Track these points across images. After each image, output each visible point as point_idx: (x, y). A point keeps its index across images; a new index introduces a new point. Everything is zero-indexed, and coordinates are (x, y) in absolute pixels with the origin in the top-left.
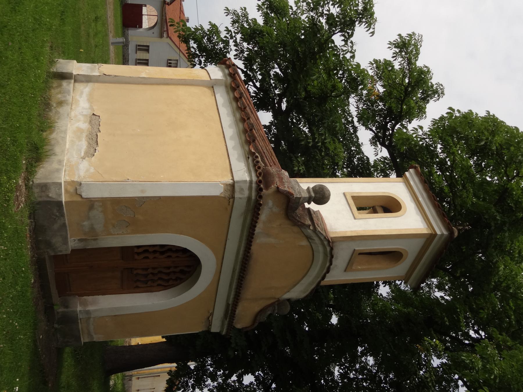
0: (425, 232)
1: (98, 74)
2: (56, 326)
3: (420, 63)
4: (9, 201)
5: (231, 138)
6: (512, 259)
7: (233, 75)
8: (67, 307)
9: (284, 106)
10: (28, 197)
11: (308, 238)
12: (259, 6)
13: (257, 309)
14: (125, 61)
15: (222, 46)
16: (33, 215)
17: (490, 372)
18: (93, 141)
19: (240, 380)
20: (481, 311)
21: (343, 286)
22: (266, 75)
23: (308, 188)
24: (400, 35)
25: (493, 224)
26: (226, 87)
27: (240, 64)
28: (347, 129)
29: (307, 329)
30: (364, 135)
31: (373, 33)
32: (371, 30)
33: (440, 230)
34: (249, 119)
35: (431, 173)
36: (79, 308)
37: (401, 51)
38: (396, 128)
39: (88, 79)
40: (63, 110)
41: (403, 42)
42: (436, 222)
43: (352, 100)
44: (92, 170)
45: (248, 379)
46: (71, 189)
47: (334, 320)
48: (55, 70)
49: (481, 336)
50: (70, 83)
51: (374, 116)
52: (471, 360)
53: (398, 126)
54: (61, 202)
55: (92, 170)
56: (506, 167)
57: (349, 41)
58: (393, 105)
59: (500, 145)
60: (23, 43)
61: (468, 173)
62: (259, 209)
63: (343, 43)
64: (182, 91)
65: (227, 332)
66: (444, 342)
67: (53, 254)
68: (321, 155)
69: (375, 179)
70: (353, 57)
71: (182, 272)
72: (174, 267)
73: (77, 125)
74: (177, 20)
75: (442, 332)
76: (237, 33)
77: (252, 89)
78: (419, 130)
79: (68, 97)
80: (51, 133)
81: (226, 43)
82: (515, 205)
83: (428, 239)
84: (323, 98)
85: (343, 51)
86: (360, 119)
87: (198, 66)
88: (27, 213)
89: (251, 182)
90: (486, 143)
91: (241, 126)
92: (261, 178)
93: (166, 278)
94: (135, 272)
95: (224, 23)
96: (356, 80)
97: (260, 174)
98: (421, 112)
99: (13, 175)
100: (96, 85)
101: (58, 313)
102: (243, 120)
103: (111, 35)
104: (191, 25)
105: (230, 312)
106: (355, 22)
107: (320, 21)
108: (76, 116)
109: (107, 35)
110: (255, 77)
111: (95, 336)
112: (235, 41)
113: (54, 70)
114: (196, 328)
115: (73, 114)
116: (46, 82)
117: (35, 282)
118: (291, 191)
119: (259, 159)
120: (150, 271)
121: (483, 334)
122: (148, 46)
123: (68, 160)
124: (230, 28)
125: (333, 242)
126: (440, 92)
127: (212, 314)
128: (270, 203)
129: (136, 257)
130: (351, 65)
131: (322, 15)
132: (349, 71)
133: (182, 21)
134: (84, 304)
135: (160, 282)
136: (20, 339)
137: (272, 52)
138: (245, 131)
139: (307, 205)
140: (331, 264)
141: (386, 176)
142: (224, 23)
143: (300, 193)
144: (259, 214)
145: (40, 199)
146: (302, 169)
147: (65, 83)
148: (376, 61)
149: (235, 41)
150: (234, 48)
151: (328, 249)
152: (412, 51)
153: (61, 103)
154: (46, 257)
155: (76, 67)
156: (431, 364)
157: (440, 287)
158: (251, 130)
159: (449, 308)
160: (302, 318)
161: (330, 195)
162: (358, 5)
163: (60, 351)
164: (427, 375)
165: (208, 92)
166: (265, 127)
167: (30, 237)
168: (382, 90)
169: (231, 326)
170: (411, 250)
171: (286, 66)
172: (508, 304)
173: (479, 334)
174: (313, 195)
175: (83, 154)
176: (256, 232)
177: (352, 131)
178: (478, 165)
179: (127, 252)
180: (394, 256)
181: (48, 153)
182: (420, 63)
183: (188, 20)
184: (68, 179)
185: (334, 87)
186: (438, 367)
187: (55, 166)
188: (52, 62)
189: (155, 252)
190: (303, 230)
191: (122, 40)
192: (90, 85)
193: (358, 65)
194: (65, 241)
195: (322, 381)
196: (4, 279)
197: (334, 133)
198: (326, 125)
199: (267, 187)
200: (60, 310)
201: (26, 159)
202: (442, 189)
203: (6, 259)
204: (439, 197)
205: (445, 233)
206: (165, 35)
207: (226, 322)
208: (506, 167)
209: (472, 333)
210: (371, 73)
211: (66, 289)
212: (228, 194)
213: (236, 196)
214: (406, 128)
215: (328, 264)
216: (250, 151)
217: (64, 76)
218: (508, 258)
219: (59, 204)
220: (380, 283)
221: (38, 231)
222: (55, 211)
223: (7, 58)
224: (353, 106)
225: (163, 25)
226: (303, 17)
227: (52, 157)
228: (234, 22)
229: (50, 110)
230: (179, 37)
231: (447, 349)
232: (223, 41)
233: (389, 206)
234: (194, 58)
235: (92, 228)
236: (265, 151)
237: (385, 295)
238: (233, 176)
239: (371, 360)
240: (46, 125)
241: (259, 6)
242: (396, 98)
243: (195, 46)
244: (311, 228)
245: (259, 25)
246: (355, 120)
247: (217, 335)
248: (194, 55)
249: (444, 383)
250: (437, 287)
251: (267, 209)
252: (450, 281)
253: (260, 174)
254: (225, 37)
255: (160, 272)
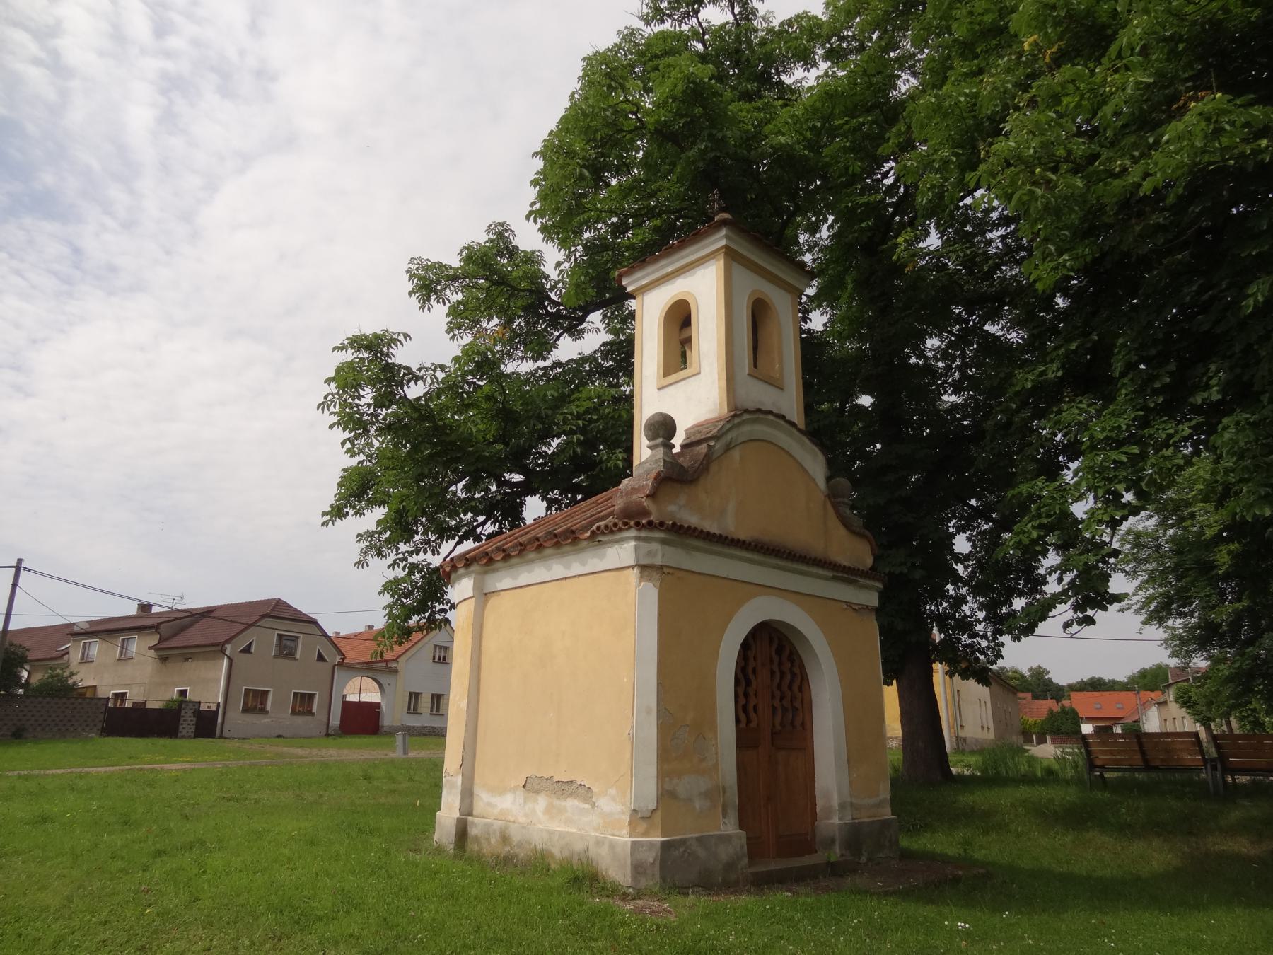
0: (722, 263)
1: (460, 777)
2: (864, 859)
3: (455, 262)
4: (658, 926)
5: (568, 567)
6: (768, 122)
7: (468, 561)
8: (833, 841)
9: (517, 478)
10: (654, 896)
11: (728, 448)
12: (355, 514)
13: (842, 531)
14: (438, 734)
15: (417, 576)
16: (683, 890)
17: (946, 162)
18: (567, 788)
19: (962, 559)
20: (850, 170)
21: (807, 387)
22: (466, 505)
23: (649, 447)
24: (410, 294)
25: (712, 155)
26: (486, 573)
27: (446, 547)
28: (555, 378)
29: (879, 446)
30: (567, 349)
31: (406, 336)
32: (401, 338)
33: (719, 240)
34: (538, 539)
35: (631, 247)
36: (836, 820)
37: (436, 292)
38: (556, 298)
39: (468, 794)
40: (516, 835)
41: (421, 288)
42: (704, 247)
43: (509, 367)
44: (613, 791)
45: (962, 544)
46: (642, 826)
47: (866, 401)
48: (452, 846)
49: (891, 168)
50: (473, 823)
51: (538, 334)
52: (929, 189)
53: (553, 296)
54: (663, 843)
55: (613, 791)
56: (622, 131)
57: (418, 373)
58: (519, 303)
59: (588, 142)
60: (410, 894)
61: (631, 189)
62: (681, 527)
63: (420, 382)
64: (489, 644)
65: (878, 580)
66: (902, 226)
67: (746, 860)
68: (597, 421)
69: (637, 333)
70: (442, 368)
71: (779, 651)
72: (772, 663)
73: (540, 814)
74: (373, 646)
75: (885, 229)
76: (398, 549)
77: (489, 528)
78: (562, 267)
79: (495, 827)
80: (552, 855)
81: (413, 568)
82: (682, 116)
83: (733, 259)
84: (506, 416)
85: (433, 383)
86: (539, 356)
87: (449, 615)
88: (680, 899)
89: (637, 539)
90: (584, 166)
91: (548, 551)
92: (632, 523)
93: (789, 677)
94: (778, 727)
95: (381, 570)
96: (483, 363)
97: (625, 524)
98: (532, 259)
99: (618, 918)
100: (477, 780)
101: (842, 855)
102: (540, 548)
103: (392, 755)
104: (380, 622)
105: (847, 574)
106: (387, 364)
107: (384, 419)
108: (526, 815)
109: (392, 761)
110: (468, 523)
111: (882, 797)
112: (411, 553)
113: (451, 848)
114: (871, 632)
115: (522, 820)
116: (470, 861)
117: (790, 890)
118: (653, 475)
119: (602, 524)
120: (777, 703)
121: (887, 166)
122: (411, 694)
123: (596, 830)
124: (390, 560)
125: (736, 409)
126: (500, 228)
127: (849, 604)
128: (672, 508)
129: (753, 725)
130: (455, 371)
131: (375, 415)
132: (465, 374)
133: (375, 639)
134: (828, 811)
135: (795, 688)
136: (880, 916)
137: (431, 496)
138: (557, 545)
139: (677, 450)
140: (770, 412)
141: (632, 315)
142: (381, 570)
143: (656, 461)
144: (689, 527)
145: (658, 877)
146: (620, 454)
147: (473, 832)
148: (450, 330)
149: (411, 553)
150: (422, 556)
151: (746, 416)
152: (436, 274)
153: (505, 839)
154: (750, 870)
155: (448, 813)
156: (936, 250)
157: (814, 229)
158: (556, 536)
159: (847, 219)
160: (860, 454)
161: (661, 414)
162: (361, 359)
163: (906, 855)
164: (954, 256)
165: (493, 601)
166: (549, 508)
167: (718, 895)
168: (495, 321)
169: (872, 573)
170: (751, 284)
171: (453, 472)
172: (841, 126)
173: (888, 172)
174: (660, 440)
175: (587, 806)
176: (717, 532)
177: (560, 370)
178: (617, 171)
179: (745, 740)
180: (759, 312)
181: (585, 861)
182: (454, 261)
183: (371, 627)
184: (626, 831)
185: (490, 398)
186: (941, 238)
187: (604, 851)
188: (439, 850)
189: (746, 695)
190: (715, 456)
191: (399, 738)
192: (477, 790)
193: (456, 359)
194: (726, 839)
195: (966, 423)
196: (781, 938)
197: (562, 400)
198: (550, 412)
199: (646, 513)
200: (836, 853)
201: (594, 897)
202: (656, 230)
203: (751, 934)
204: (666, 238)
205: (724, 232)
206: (393, 665)
207: (862, 581)
208: (622, 131)
209: (889, 181)
210: (468, 339)
211: (804, 843)
212: (656, 576)
213: (659, 563)
214: (557, 283)
215: (771, 417)
216: (589, 538)
217: (462, 833)
218: (767, 129)
219: (666, 846)
220: (805, 327)
221: (708, 883)
222: (677, 853)
223: (433, 920)
224: (519, 366)
225: (378, 668)
226: (376, 444)
227: (590, 853)
228: (380, 554)
229: (516, 855)
230: (401, 644)
231: (912, 224)
232: (411, 573)
233: (680, 319)
234: (435, 620)
235: (706, 795)
236: (589, 514)
237: (825, 319)
238: (628, 567)
239: (932, 342)
240: (539, 863)
241: (355, 514)
242: (508, 299)
243: (416, 618)
244: (712, 443)
245: (387, 515)
246: (541, 364)
247: (883, 596)
248: (431, 620)
249: (969, 228)
250: (813, 234)
251: (682, 513)
252: (804, 215)
253: (625, 524)
254: (404, 569)
255: (779, 687)
